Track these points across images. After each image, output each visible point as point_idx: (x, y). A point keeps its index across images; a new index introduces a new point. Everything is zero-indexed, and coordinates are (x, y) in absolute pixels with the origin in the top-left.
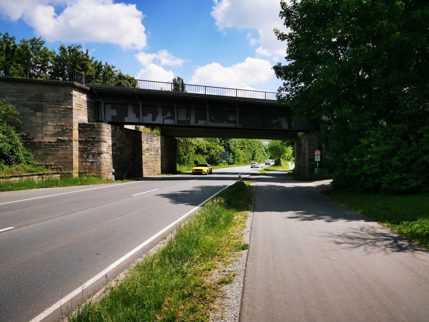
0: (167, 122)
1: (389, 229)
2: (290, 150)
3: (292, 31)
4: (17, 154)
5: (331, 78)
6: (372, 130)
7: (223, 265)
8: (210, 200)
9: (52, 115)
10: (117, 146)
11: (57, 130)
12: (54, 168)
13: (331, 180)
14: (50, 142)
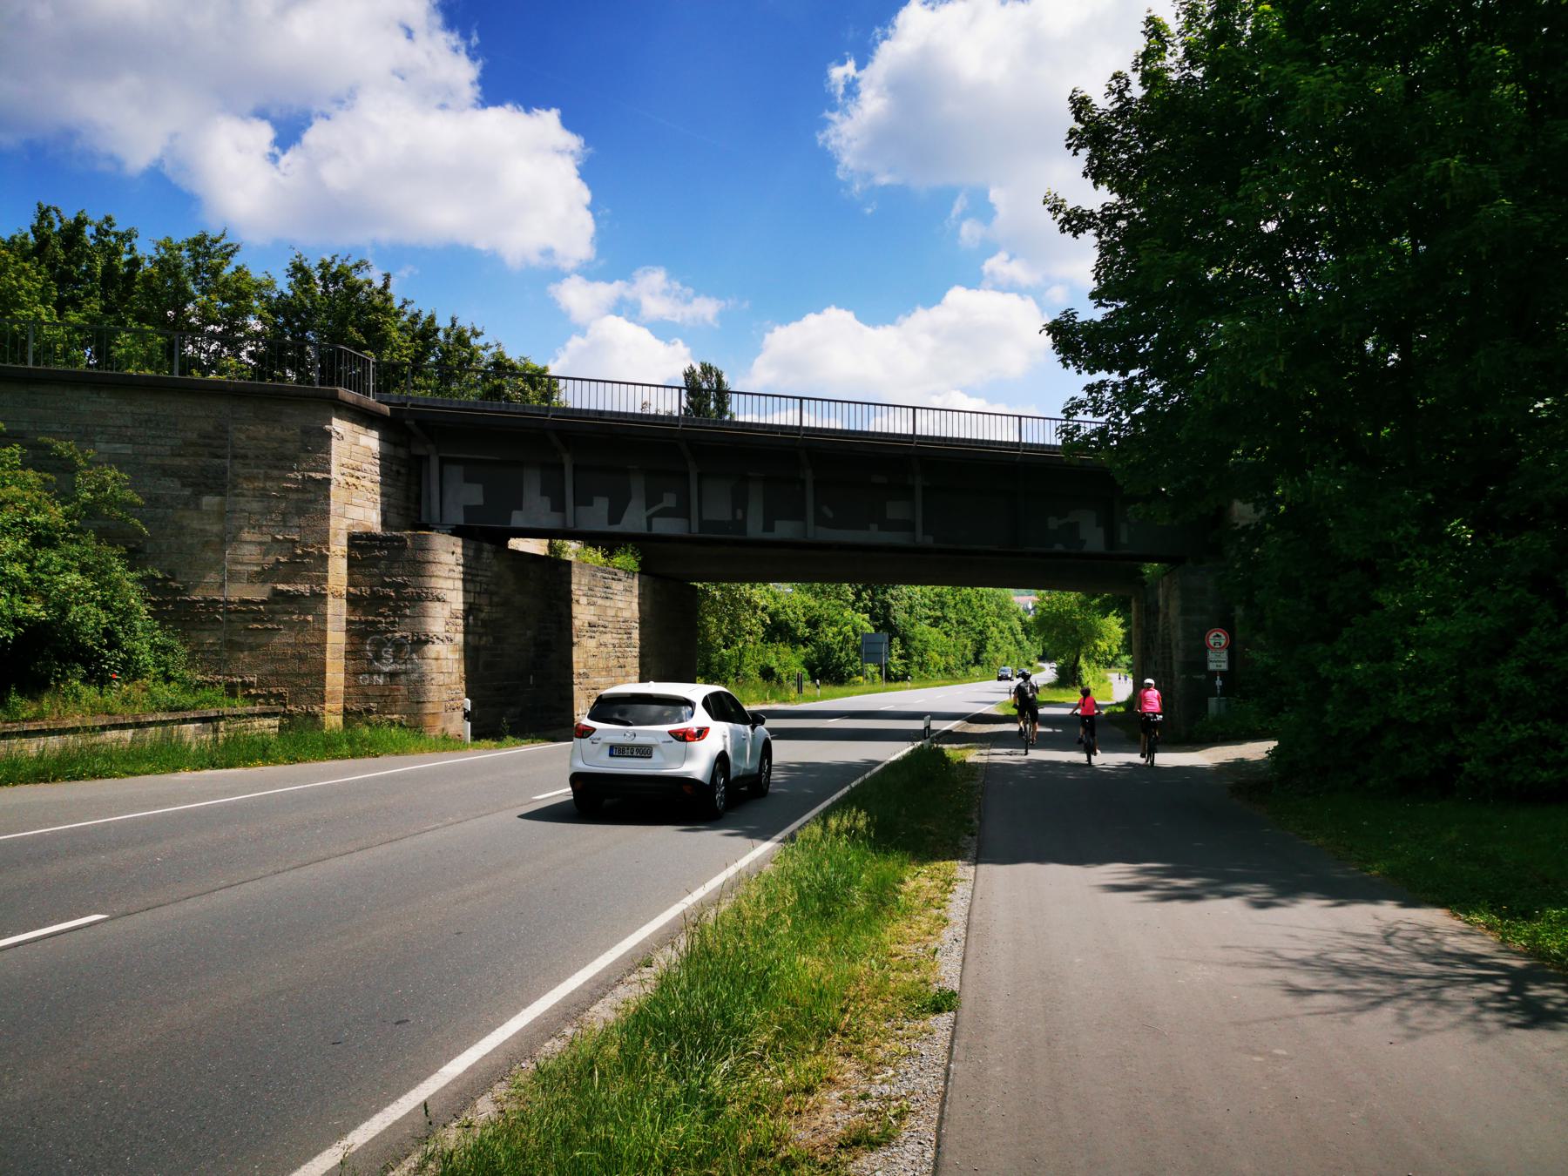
0: (663, 526)
1: (1492, 938)
2: (1113, 629)
3: (1114, 198)
4: (127, 644)
5: (1259, 367)
6: (1419, 556)
7: (859, 1072)
8: (815, 817)
9: (256, 506)
10: (482, 615)
11: (271, 559)
12: (258, 696)
13: (1276, 743)
14: (248, 602)
